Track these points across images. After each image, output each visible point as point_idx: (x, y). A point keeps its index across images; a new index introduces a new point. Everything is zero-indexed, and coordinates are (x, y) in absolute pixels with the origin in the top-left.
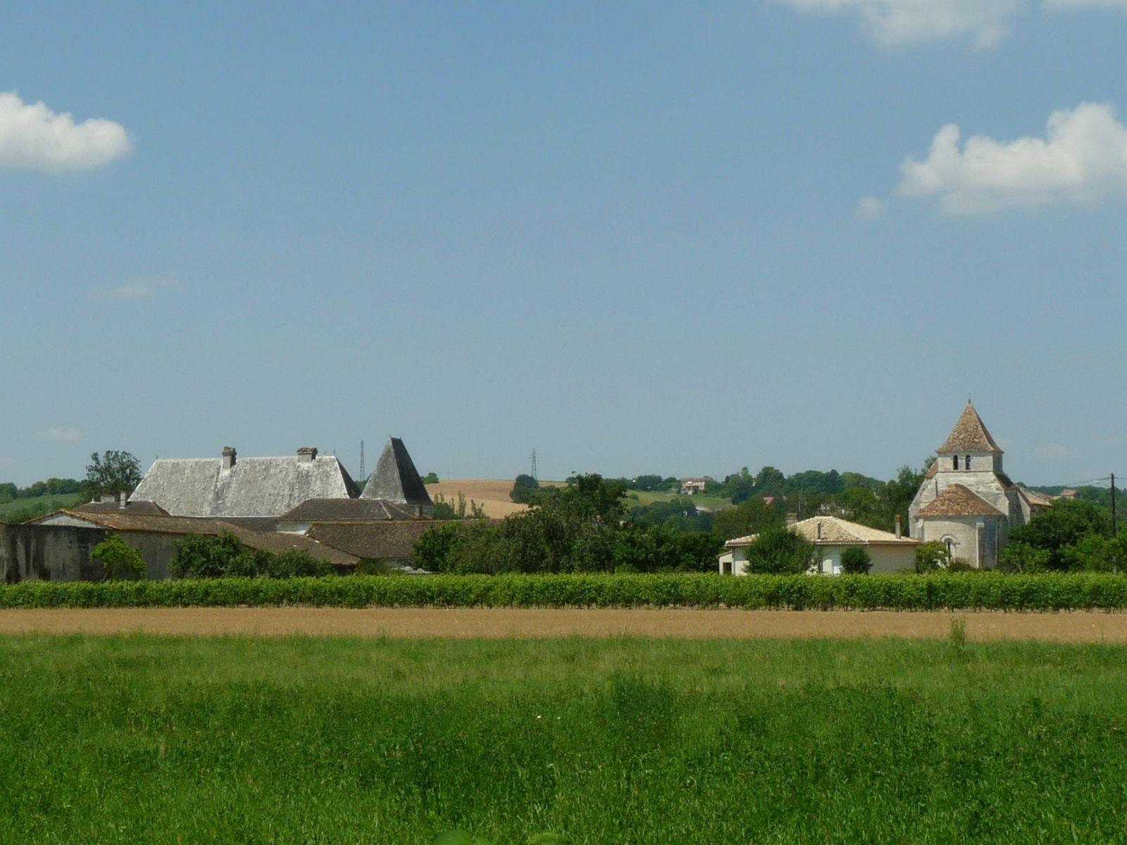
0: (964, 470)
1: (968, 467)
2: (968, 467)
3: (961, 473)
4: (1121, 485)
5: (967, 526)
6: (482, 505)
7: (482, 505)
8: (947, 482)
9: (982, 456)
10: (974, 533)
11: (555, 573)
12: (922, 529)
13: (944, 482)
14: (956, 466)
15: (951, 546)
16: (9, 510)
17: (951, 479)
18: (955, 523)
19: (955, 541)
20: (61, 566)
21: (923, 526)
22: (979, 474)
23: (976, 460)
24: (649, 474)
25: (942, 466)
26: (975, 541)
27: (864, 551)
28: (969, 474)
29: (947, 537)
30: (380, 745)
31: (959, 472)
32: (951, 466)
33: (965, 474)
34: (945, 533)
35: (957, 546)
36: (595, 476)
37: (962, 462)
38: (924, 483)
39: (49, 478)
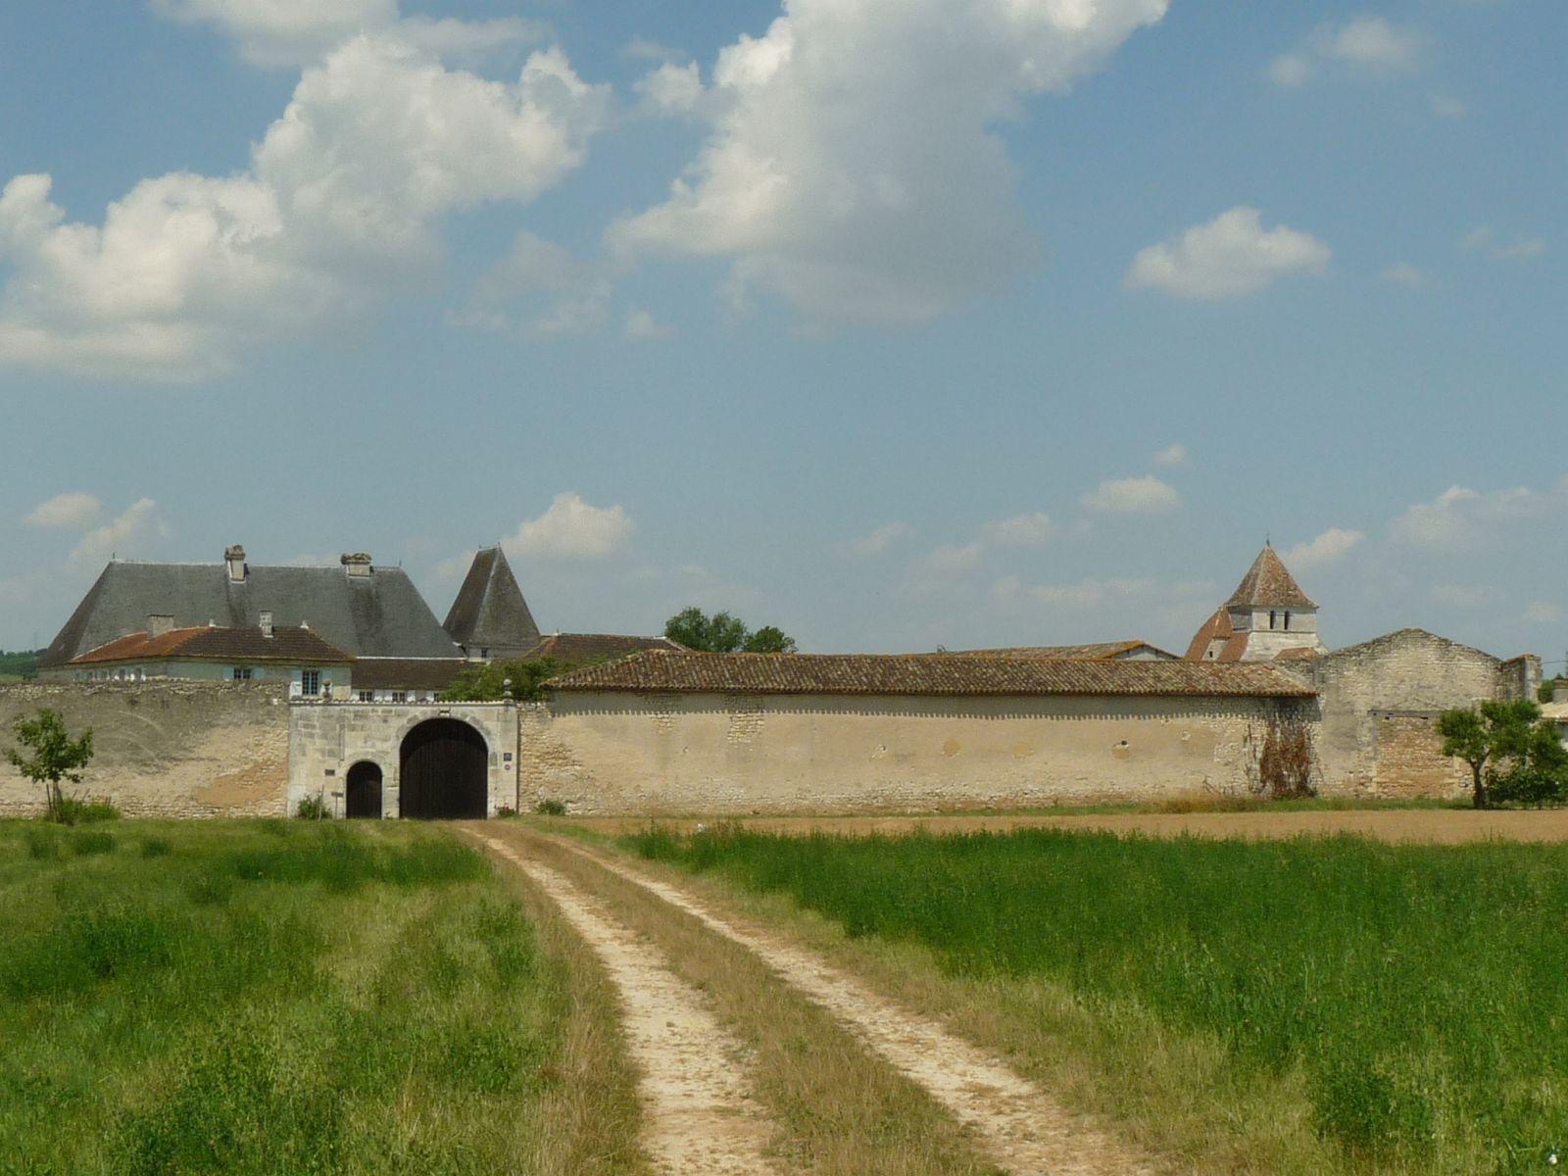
0: (1283, 629)
3: (1279, 634)
5: (345, 811)
8: (1264, 644)
9: (1305, 613)
11: (1482, 711)
13: (1261, 644)
16: (561, 1172)
17: (1269, 640)
20: (1488, 836)
22: (1300, 635)
24: (599, 633)
25: (1257, 624)
28: (1288, 635)
30: (1357, 1027)
31: (1276, 632)
33: (1284, 635)
37: (1280, 619)
38: (1211, 644)
39: (673, 616)
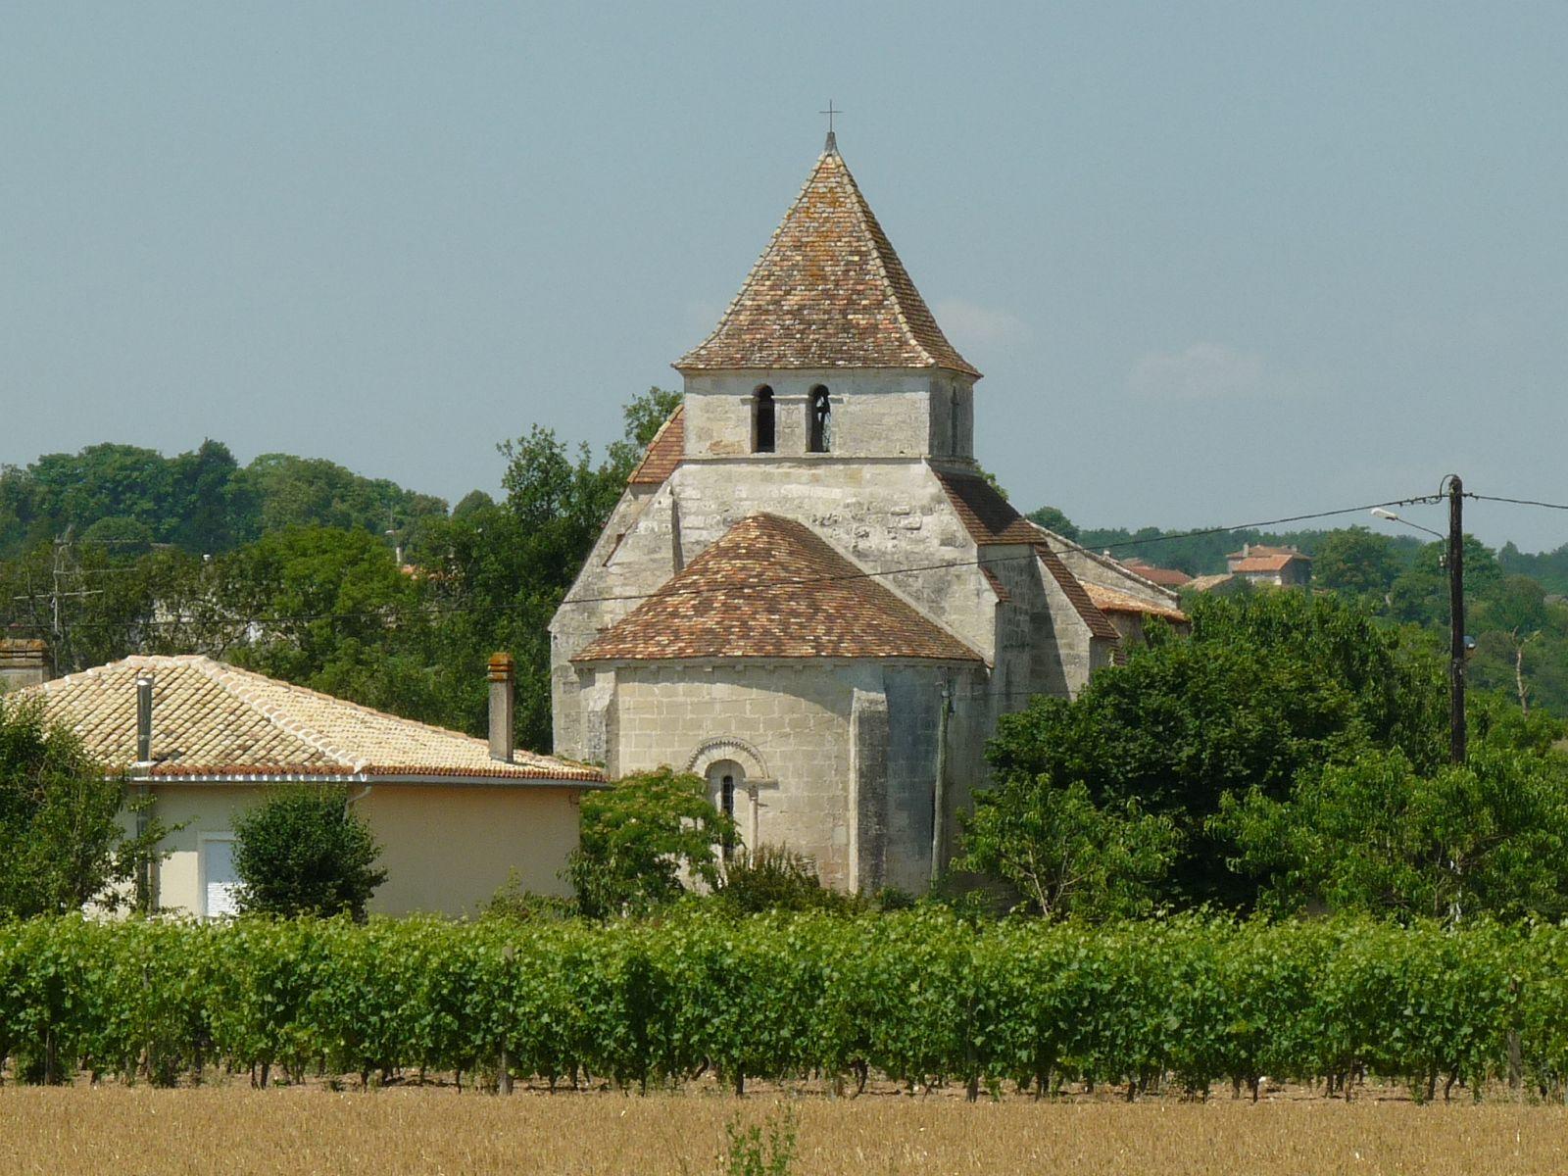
1: (817, 439)
2: (817, 439)
3: (785, 468)
10: (841, 738)
12: (611, 714)
14: (765, 435)
18: (754, 693)
23: (852, 408)
25: (704, 434)
29: (717, 754)
37: (791, 417)
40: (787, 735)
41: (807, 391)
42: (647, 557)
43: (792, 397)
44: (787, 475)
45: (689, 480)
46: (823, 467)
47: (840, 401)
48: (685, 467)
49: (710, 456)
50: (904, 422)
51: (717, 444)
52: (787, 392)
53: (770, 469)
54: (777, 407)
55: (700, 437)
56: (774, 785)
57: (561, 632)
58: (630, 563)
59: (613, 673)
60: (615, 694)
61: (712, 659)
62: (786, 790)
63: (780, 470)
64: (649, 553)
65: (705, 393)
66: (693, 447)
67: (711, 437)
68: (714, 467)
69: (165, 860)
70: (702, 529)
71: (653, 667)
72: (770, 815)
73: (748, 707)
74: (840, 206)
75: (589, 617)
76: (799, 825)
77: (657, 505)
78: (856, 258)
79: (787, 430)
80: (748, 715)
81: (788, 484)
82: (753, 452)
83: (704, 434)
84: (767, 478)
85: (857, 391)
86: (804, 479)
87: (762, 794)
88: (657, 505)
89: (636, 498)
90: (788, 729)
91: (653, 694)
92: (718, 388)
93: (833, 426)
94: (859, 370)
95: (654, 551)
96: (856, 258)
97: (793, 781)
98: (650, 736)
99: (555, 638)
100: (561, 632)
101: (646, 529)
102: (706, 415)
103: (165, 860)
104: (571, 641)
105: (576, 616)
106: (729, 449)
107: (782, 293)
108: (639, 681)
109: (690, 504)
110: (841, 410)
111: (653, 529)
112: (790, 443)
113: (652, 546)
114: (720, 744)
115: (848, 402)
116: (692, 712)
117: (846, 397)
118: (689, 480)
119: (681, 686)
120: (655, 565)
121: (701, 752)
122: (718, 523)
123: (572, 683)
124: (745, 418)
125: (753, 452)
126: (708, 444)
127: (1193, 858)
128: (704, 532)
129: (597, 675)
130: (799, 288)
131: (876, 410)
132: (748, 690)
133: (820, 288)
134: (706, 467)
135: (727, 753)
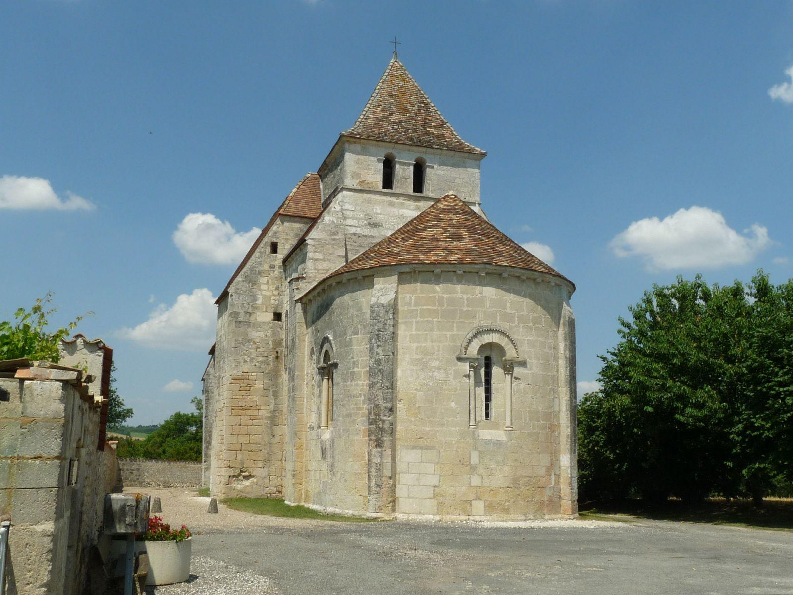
1: (418, 186)
2: (418, 186)
3: (401, 200)
4: (777, 281)
6: (117, 389)
7: (117, 389)
10: (556, 337)
12: (394, 308)
14: (388, 182)
15: (496, 371)
18: (512, 297)
19: (511, 353)
21: (396, 298)
23: (439, 172)
25: (356, 175)
26: (556, 359)
27: (125, 541)
29: (487, 338)
32: (379, 179)
34: (486, 323)
35: (518, 371)
36: (176, 414)
37: (404, 173)
40: (531, 328)
41: (414, 159)
42: (329, 237)
43: (402, 161)
44: (403, 204)
45: (347, 200)
46: (422, 202)
47: (433, 167)
48: (345, 192)
49: (359, 188)
50: (467, 183)
51: (363, 182)
52: (402, 159)
53: (394, 199)
54: (398, 166)
55: (353, 176)
56: (523, 364)
57: (236, 292)
58: (320, 239)
59: (397, 276)
60: (397, 292)
61: (488, 266)
62: (531, 369)
63: (398, 201)
64: (330, 235)
65: (358, 154)
66: (349, 182)
67: (360, 178)
68: (361, 195)
69: (174, 415)
70: (357, 227)
71: (438, 271)
72: (522, 386)
73: (508, 305)
74: (407, 82)
75: (252, 286)
76: (538, 395)
77: (333, 209)
78: (423, 105)
79: (403, 179)
80: (508, 311)
81: (403, 209)
82: (383, 188)
83: (356, 175)
84: (391, 204)
85: (442, 164)
86: (412, 207)
87: (518, 371)
88: (333, 209)
89: (283, 224)
90: (531, 324)
91: (435, 291)
92: (364, 152)
93: (428, 180)
94: (444, 151)
95: (333, 234)
96: (423, 105)
97: (534, 362)
98: (429, 322)
99: (232, 295)
100: (236, 292)
101: (329, 221)
102: (357, 165)
103: (174, 415)
104: (241, 298)
105: (245, 284)
106: (370, 186)
107: (388, 114)
108: (422, 282)
109: (348, 213)
110: (433, 172)
111: (333, 221)
112: (405, 187)
113: (333, 230)
114: (491, 331)
115: (437, 168)
116: (468, 306)
117: (436, 166)
118: (347, 200)
119: (459, 287)
120: (334, 243)
121: (475, 336)
122: (366, 224)
123: (241, 322)
124: (380, 169)
125: (383, 188)
126: (358, 181)
127: (676, 429)
128: (359, 229)
129: (375, 279)
130: (396, 113)
131: (452, 175)
132: (508, 294)
133: (408, 115)
134: (357, 195)
135: (494, 338)
